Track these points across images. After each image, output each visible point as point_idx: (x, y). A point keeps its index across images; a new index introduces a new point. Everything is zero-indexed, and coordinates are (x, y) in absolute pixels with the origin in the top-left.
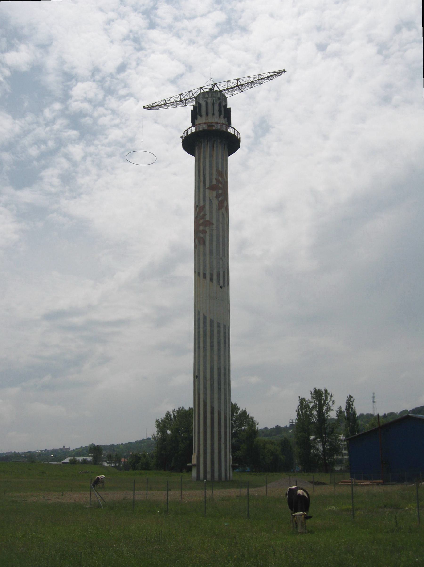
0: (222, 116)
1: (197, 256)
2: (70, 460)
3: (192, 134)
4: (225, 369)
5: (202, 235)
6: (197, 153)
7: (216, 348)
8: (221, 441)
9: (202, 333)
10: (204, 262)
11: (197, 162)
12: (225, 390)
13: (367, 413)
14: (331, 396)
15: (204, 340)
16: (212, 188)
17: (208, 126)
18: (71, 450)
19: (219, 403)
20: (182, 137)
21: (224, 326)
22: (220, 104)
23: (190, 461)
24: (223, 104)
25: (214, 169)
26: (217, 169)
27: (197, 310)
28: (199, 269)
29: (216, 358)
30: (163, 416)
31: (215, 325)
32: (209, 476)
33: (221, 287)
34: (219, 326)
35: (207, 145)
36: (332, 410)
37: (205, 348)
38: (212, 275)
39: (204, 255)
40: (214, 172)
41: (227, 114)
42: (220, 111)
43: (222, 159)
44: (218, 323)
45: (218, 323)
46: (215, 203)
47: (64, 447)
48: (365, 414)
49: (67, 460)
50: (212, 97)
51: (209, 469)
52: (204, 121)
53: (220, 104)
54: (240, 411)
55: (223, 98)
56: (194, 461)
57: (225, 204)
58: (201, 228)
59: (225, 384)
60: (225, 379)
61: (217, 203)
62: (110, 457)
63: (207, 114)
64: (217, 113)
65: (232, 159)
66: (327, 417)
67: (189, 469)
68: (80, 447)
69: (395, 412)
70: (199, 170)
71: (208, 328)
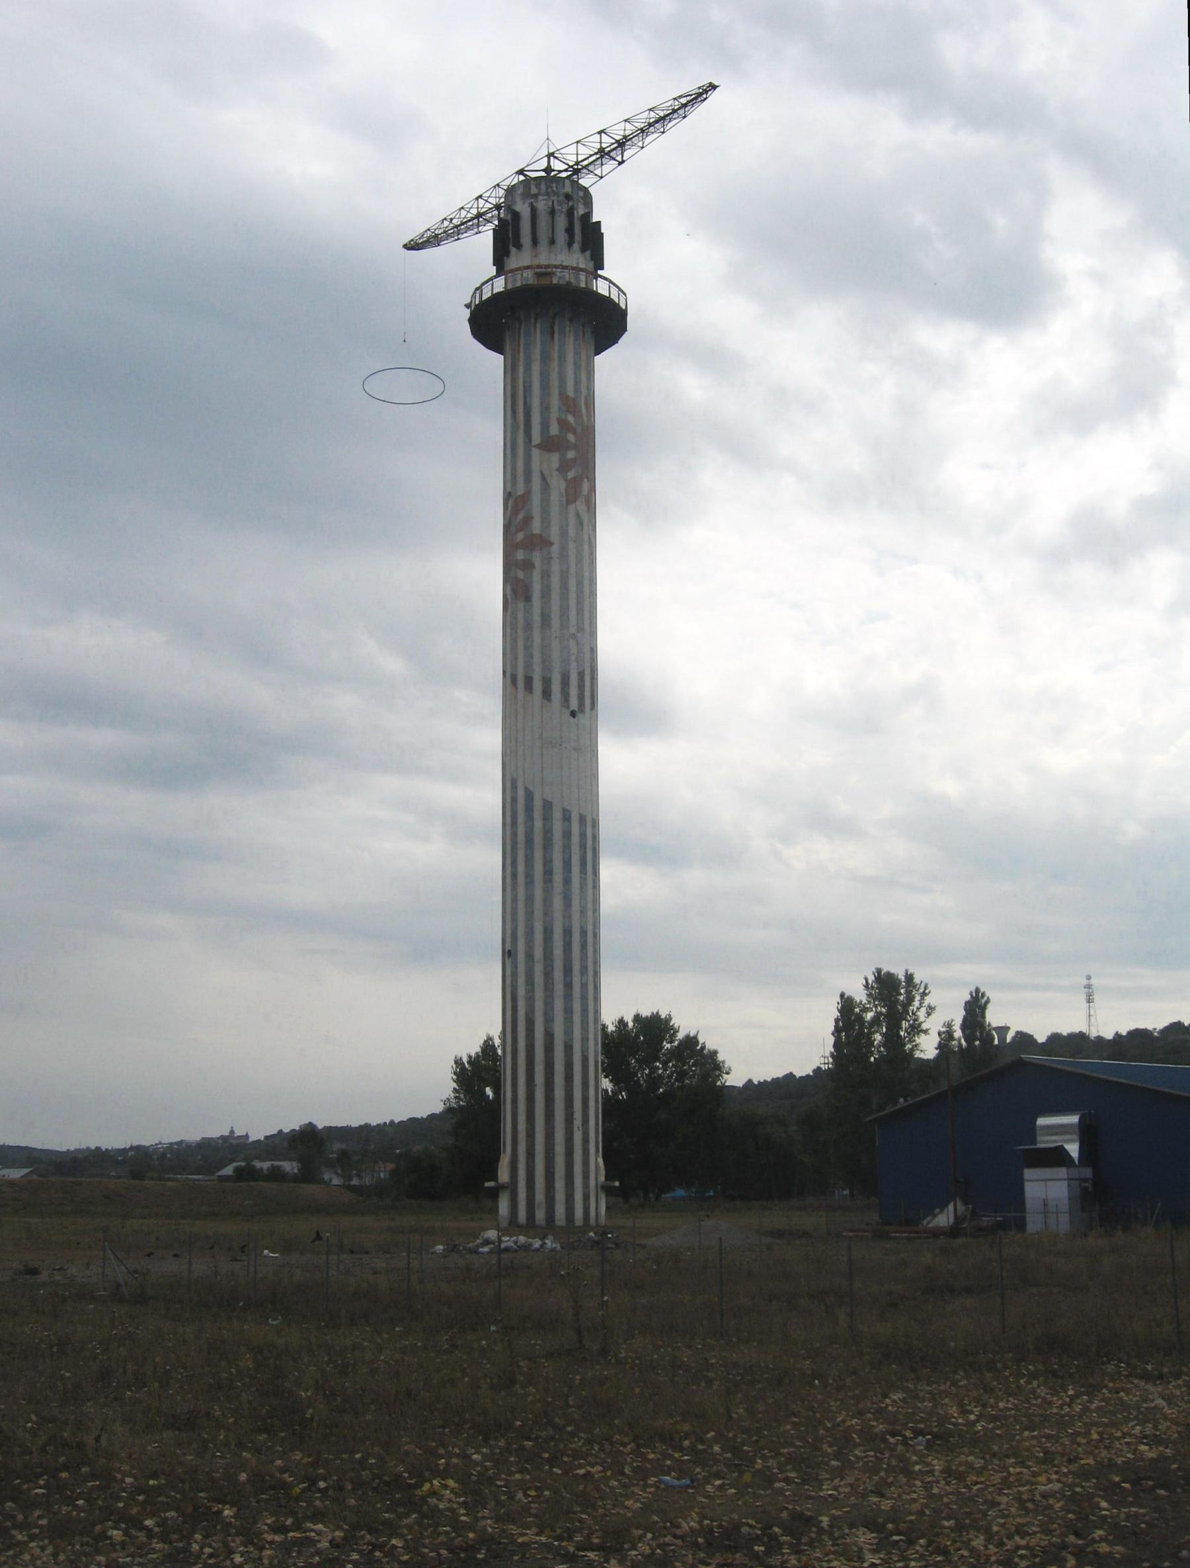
0: (576, 246)
1: (509, 630)
2: (237, 1170)
3: (496, 297)
4: (584, 933)
5: (520, 575)
6: (508, 347)
7: (558, 878)
8: (572, 1123)
9: (521, 837)
10: (528, 648)
11: (511, 371)
12: (584, 986)
13: (1069, 1031)
14: (924, 994)
15: (526, 856)
16: (549, 445)
17: (538, 275)
18: (251, 1140)
19: (568, 1019)
20: (468, 306)
21: (582, 819)
22: (570, 213)
23: (494, 1177)
24: (581, 211)
25: (555, 391)
26: (563, 395)
27: (508, 777)
28: (515, 666)
29: (558, 902)
30: (475, 1048)
31: (557, 814)
32: (540, 1216)
33: (573, 714)
34: (567, 818)
35: (535, 327)
36: (926, 1032)
37: (529, 876)
38: (547, 682)
39: (528, 626)
40: (555, 402)
41: (591, 240)
42: (570, 231)
43: (577, 366)
44: (564, 810)
45: (564, 810)
46: (558, 485)
47: (232, 1132)
48: (1065, 1034)
49: (228, 1171)
50: (547, 194)
51: (540, 1197)
52: (527, 263)
53: (570, 213)
54: (680, 1035)
55: (581, 194)
56: (504, 1176)
57: (585, 487)
58: (520, 555)
59: (584, 970)
60: (584, 957)
61: (563, 485)
62: (344, 1161)
63: (535, 242)
64: (561, 237)
65: (606, 363)
66: (912, 1050)
67: (494, 1194)
68: (275, 1132)
69: (1150, 1028)
70: (514, 396)
71: (538, 824)
